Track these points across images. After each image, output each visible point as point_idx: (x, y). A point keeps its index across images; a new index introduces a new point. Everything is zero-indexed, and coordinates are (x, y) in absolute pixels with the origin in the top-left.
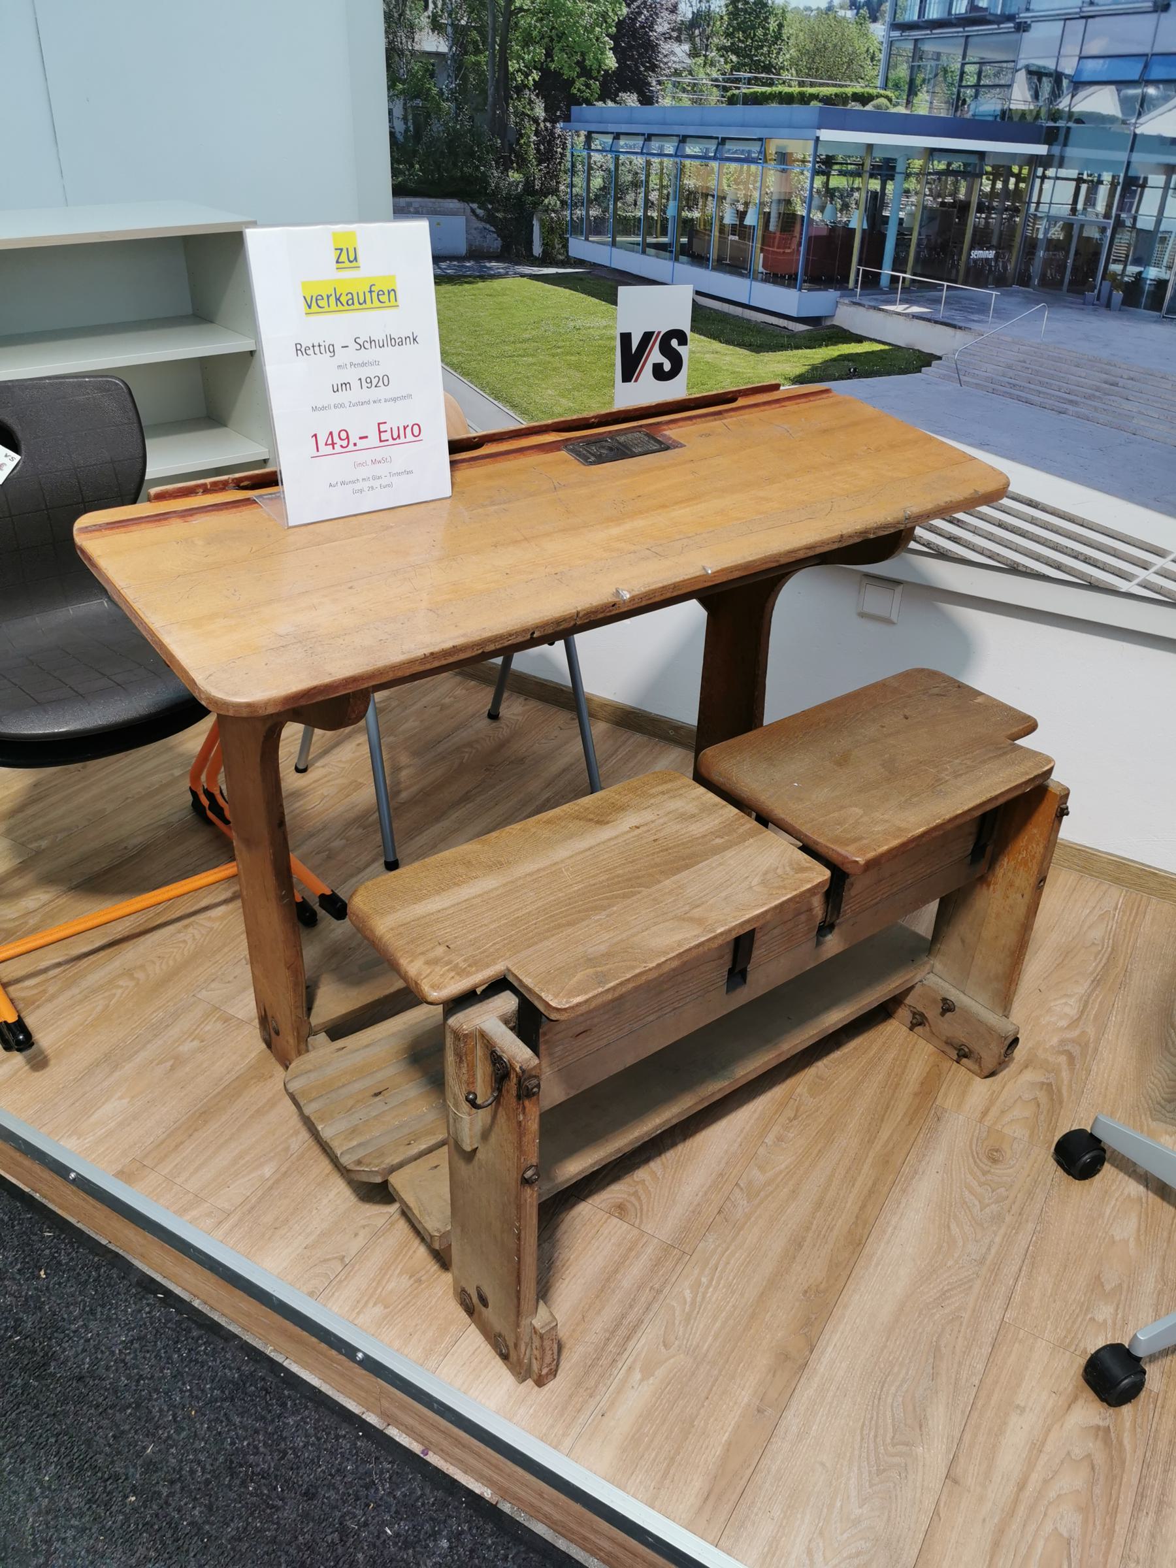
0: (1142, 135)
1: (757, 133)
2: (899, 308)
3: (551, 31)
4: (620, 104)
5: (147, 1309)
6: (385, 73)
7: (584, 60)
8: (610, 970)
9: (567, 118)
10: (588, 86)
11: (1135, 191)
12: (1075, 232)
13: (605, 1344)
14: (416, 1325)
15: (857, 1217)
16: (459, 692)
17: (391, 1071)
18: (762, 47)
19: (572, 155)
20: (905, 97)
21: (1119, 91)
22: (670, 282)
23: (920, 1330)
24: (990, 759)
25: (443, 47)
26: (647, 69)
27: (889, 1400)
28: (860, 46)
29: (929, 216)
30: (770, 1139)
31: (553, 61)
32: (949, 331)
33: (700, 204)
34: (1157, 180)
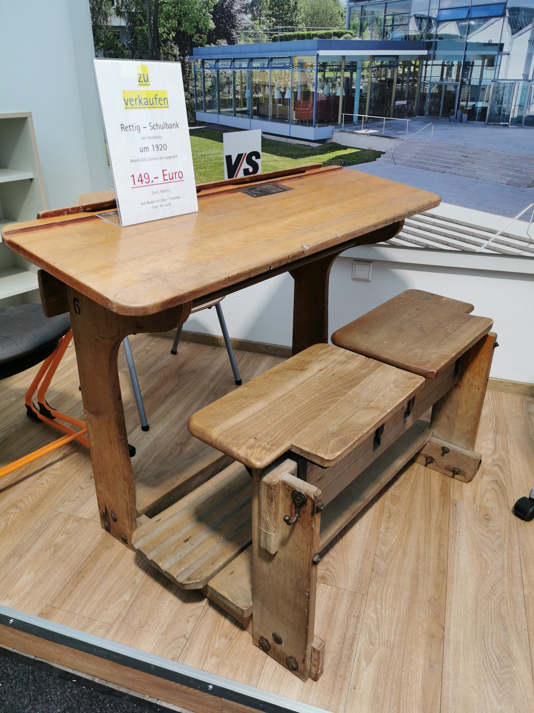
0: (470, 43)
1: (288, 54)
2: (363, 131)
3: (180, 12)
4: (218, 45)
5: (69, 690)
6: (93, 38)
7: (198, 25)
8: (346, 437)
9: (191, 54)
10: (201, 38)
11: (469, 68)
12: (443, 89)
13: (341, 651)
14: (238, 663)
15: (438, 559)
18: (287, 14)
19: (195, 71)
20: (359, 33)
21: (458, 24)
22: (250, 129)
23: (489, 608)
24: (464, 322)
25: (123, 23)
26: (231, 28)
27: (490, 646)
28: (336, 10)
29: (374, 87)
30: (382, 529)
31: (182, 26)
32: (388, 140)
33: (262, 90)
34: (478, 62)
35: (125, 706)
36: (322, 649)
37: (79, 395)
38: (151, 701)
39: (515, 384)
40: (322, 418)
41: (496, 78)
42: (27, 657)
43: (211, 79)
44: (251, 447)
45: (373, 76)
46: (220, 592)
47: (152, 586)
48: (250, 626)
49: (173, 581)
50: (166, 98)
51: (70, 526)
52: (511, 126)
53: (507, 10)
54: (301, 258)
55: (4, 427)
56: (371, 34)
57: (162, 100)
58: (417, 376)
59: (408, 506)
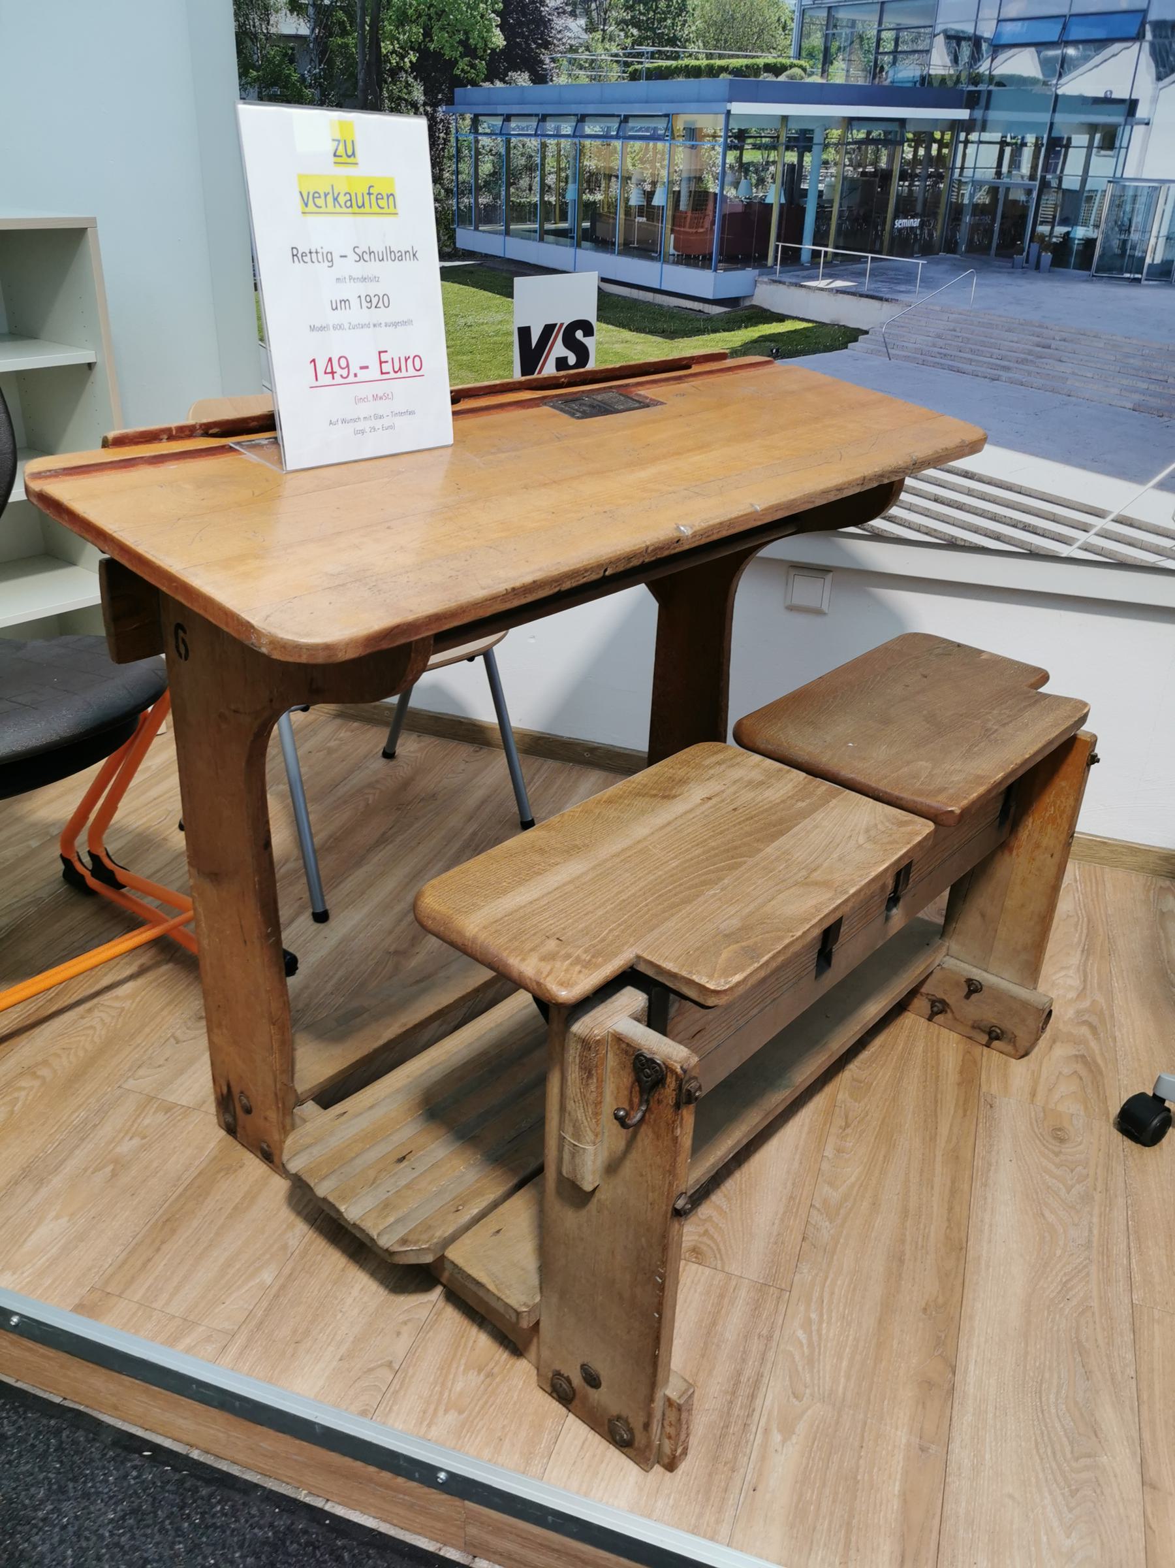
0: (1064, 96)
2: (822, 283)
3: (429, 9)
5: (134, 1473)
7: (468, 39)
8: (756, 943)
9: (450, 101)
10: (473, 66)
12: (1001, 196)
14: (504, 1427)
15: (949, 1220)
16: (343, 734)
17: (408, 1131)
18: (665, 19)
19: (457, 140)
20: (820, 66)
21: (1039, 53)
22: (572, 270)
23: (1055, 1328)
24: (1025, 707)
25: (304, 30)
26: (539, 46)
28: (771, 15)
29: (850, 186)
30: (829, 1152)
31: (432, 41)
33: (603, 185)
34: (1081, 139)
35: (254, 1511)
36: (687, 1401)
37: (179, 840)
38: (312, 1503)
39: (1133, 850)
40: (706, 902)
41: (1118, 175)
42: (44, 1399)
43: (491, 157)
44: (550, 957)
45: (847, 163)
46: (470, 1272)
47: (324, 1255)
48: (533, 1349)
49: (369, 1245)
50: (392, 195)
51: (150, 1120)
52: (1146, 282)
53: (1148, 27)
54: (673, 552)
55: (13, 904)
56: (848, 71)
57: (320, 197)
58: (916, 818)
59: (887, 1103)
